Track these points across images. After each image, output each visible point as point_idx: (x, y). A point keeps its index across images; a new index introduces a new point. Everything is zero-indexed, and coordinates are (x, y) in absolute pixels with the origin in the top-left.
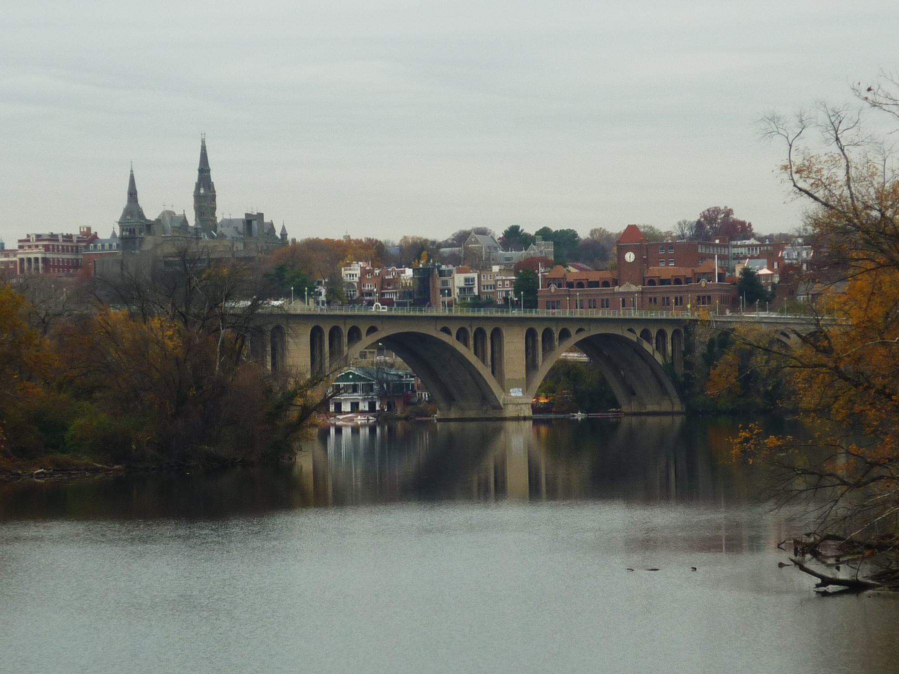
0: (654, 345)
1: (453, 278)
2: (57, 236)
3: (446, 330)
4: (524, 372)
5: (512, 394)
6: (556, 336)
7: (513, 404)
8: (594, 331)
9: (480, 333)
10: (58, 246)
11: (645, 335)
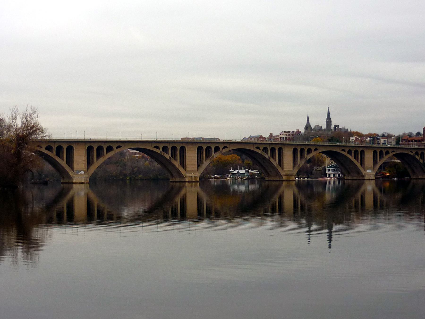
0: (420, 157)
1: (380, 140)
2: (289, 132)
3: (344, 150)
4: (372, 164)
5: (368, 172)
6: (384, 153)
7: (367, 175)
8: (398, 152)
9: (356, 152)
10: (290, 134)
11: (417, 153)
